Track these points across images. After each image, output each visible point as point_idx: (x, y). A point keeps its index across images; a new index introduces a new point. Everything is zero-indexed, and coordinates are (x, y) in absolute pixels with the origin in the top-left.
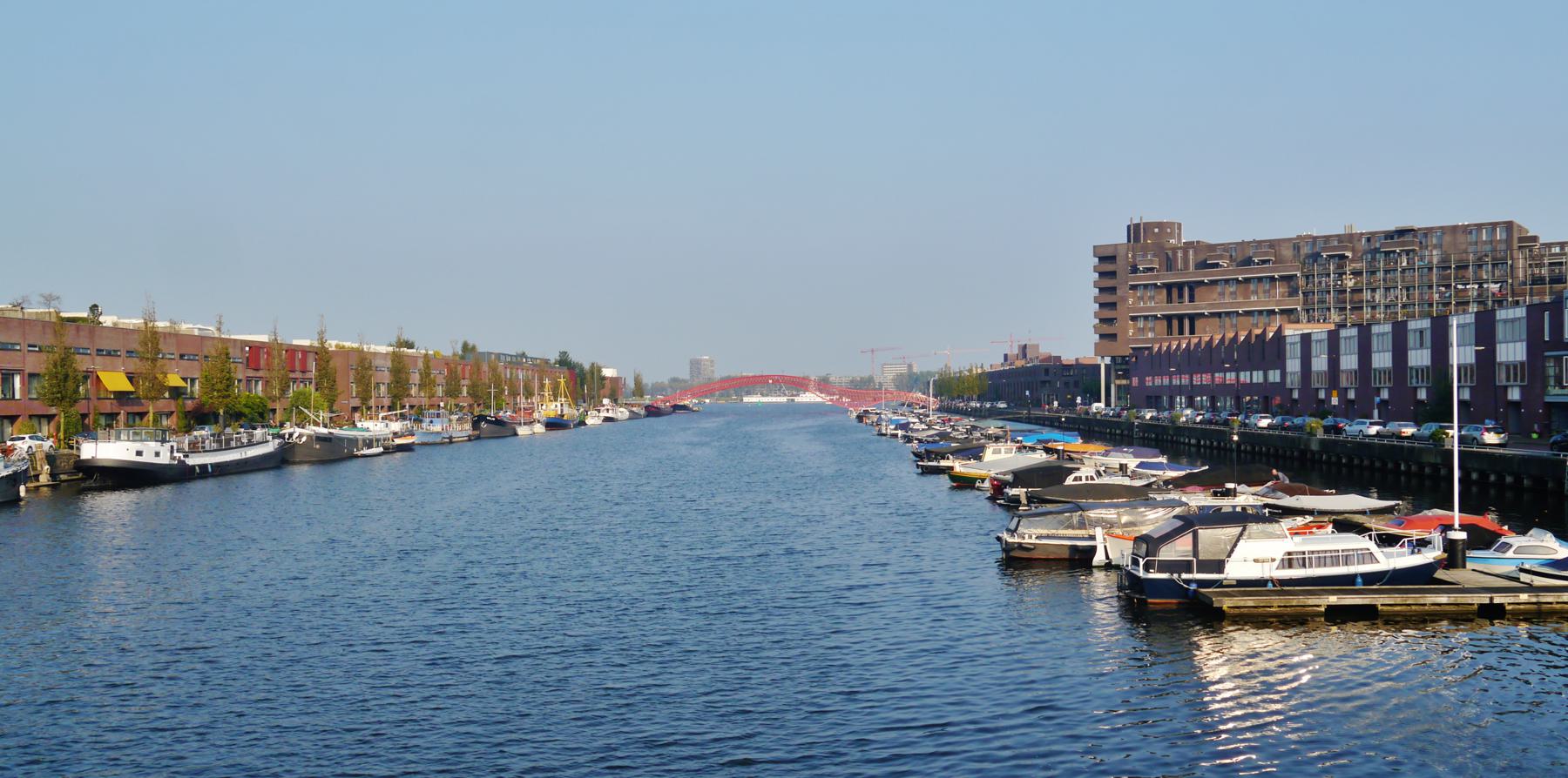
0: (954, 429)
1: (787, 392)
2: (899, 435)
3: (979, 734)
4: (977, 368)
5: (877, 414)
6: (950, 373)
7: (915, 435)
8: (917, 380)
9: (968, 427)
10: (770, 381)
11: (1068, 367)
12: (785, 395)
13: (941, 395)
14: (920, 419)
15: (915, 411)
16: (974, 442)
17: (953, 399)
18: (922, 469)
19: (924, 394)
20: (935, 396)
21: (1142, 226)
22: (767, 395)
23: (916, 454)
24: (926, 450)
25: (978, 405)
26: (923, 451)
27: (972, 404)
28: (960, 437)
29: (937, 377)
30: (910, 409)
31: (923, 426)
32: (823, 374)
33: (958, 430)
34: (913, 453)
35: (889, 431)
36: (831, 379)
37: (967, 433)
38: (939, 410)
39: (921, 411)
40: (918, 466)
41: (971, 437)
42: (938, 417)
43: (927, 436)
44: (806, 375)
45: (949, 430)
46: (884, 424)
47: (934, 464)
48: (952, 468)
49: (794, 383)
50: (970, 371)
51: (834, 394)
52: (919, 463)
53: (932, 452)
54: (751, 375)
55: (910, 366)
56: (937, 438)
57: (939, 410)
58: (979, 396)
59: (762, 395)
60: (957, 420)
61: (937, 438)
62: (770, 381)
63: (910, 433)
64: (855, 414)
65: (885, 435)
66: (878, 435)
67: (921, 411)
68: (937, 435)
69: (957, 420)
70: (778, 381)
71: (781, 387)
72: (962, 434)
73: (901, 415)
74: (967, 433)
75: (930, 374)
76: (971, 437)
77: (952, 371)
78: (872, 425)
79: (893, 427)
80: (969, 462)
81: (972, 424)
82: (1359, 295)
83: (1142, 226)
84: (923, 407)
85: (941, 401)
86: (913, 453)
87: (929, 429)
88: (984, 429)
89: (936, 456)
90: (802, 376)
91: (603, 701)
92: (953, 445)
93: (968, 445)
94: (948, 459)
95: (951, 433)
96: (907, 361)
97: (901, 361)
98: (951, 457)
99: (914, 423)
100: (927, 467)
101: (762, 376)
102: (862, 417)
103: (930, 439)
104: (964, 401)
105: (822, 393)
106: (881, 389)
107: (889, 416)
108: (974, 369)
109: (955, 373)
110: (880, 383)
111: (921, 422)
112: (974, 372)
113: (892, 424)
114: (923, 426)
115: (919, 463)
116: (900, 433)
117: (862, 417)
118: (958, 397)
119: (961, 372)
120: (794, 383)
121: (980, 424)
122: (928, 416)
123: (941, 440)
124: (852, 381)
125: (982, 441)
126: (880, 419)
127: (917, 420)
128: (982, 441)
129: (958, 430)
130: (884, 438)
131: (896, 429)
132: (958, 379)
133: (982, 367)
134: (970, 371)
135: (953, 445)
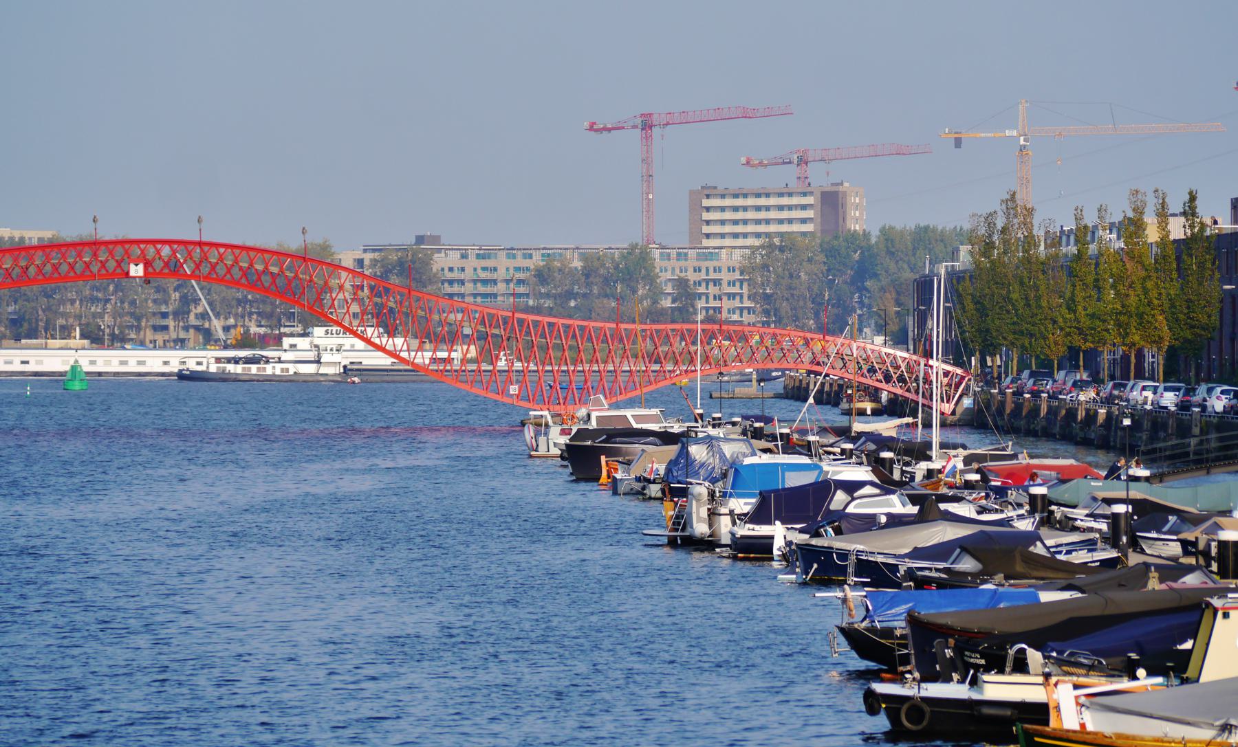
0: (1048, 521)
1: (217, 325)
2: (778, 543)
3: (1133, 688)
4: (1163, 215)
5: (666, 438)
6: (1030, 241)
7: (853, 544)
8: (863, 272)
9: (1120, 509)
10: (137, 270)
11: (706, 550)
12: (208, 338)
13: (989, 348)
14: (879, 465)
15: (858, 426)
16: (1154, 584)
17: (1045, 369)
18: (893, 716)
19: (899, 340)
20: (956, 353)
21: (1132, 374)
22: (118, 340)
23: (858, 640)
24: (913, 620)
25: (1169, 400)
26: (900, 626)
27: (1143, 395)
28: (1080, 557)
29: (965, 258)
30: (833, 417)
31: (897, 505)
32: (401, 236)
33: (1067, 525)
34: (851, 635)
35: (725, 526)
36: (441, 262)
37: (1112, 539)
38: (976, 421)
39: (887, 427)
40: (873, 702)
41: (1134, 559)
42: (968, 461)
43: (917, 553)
44: (315, 238)
45: (1025, 525)
46: (700, 489)
47: (954, 690)
48: (1039, 712)
49: (250, 280)
50: (1132, 227)
51: (452, 338)
52: (881, 688)
53: (944, 631)
54: (33, 236)
55: (832, 202)
56: (968, 564)
57: (976, 421)
58: (1172, 356)
59: (95, 338)
60: (1064, 478)
61: (968, 564)
62: (137, 270)
63: (829, 540)
64: (557, 439)
65: (708, 544)
66: (672, 543)
67: (887, 427)
68: (964, 546)
69: (1064, 478)
70: (173, 269)
71: (188, 301)
72: (1090, 545)
73: (789, 446)
74: (1112, 539)
75: (924, 238)
76: (1134, 559)
77: (1039, 232)
78: (640, 494)
79: (743, 505)
80: (1124, 684)
81: (1137, 492)
82: (945, 440)
83: (1132, 374)
84: (895, 408)
85: (987, 378)
86: (851, 635)
87: (920, 519)
88: (1196, 520)
89: (958, 650)
90: (293, 244)
91: (787, 663)
92: (1046, 597)
93: (1124, 600)
94: (1021, 666)
95: (1033, 537)
96: (820, 178)
97: (789, 175)
98: (1034, 657)
99: (851, 487)
100: (917, 707)
101: (95, 245)
102: (594, 453)
103: (933, 568)
104: (1096, 380)
105: (391, 333)
106: (683, 313)
107: (728, 450)
108: (1150, 219)
109: (1055, 241)
110: (682, 283)
111: (887, 485)
112: (1152, 235)
113: (738, 489)
114: (897, 505)
115: (881, 688)
116: (779, 533)
117: (594, 453)
118: (1071, 359)
119: (1083, 234)
120: (250, 280)
121: (1173, 494)
122: (921, 452)
123: (985, 574)
124: (542, 276)
125: (1192, 580)
126: (683, 462)
127: (862, 473)
128: (1192, 580)
129: (1067, 525)
130: (699, 559)
131: (758, 516)
132: (1073, 268)
133: (1190, 212)
134: (1132, 227)
135: (1046, 597)
